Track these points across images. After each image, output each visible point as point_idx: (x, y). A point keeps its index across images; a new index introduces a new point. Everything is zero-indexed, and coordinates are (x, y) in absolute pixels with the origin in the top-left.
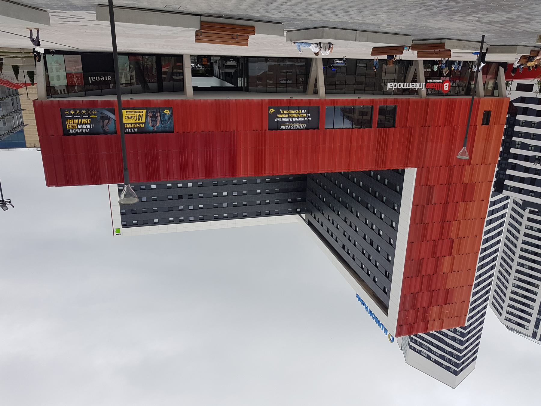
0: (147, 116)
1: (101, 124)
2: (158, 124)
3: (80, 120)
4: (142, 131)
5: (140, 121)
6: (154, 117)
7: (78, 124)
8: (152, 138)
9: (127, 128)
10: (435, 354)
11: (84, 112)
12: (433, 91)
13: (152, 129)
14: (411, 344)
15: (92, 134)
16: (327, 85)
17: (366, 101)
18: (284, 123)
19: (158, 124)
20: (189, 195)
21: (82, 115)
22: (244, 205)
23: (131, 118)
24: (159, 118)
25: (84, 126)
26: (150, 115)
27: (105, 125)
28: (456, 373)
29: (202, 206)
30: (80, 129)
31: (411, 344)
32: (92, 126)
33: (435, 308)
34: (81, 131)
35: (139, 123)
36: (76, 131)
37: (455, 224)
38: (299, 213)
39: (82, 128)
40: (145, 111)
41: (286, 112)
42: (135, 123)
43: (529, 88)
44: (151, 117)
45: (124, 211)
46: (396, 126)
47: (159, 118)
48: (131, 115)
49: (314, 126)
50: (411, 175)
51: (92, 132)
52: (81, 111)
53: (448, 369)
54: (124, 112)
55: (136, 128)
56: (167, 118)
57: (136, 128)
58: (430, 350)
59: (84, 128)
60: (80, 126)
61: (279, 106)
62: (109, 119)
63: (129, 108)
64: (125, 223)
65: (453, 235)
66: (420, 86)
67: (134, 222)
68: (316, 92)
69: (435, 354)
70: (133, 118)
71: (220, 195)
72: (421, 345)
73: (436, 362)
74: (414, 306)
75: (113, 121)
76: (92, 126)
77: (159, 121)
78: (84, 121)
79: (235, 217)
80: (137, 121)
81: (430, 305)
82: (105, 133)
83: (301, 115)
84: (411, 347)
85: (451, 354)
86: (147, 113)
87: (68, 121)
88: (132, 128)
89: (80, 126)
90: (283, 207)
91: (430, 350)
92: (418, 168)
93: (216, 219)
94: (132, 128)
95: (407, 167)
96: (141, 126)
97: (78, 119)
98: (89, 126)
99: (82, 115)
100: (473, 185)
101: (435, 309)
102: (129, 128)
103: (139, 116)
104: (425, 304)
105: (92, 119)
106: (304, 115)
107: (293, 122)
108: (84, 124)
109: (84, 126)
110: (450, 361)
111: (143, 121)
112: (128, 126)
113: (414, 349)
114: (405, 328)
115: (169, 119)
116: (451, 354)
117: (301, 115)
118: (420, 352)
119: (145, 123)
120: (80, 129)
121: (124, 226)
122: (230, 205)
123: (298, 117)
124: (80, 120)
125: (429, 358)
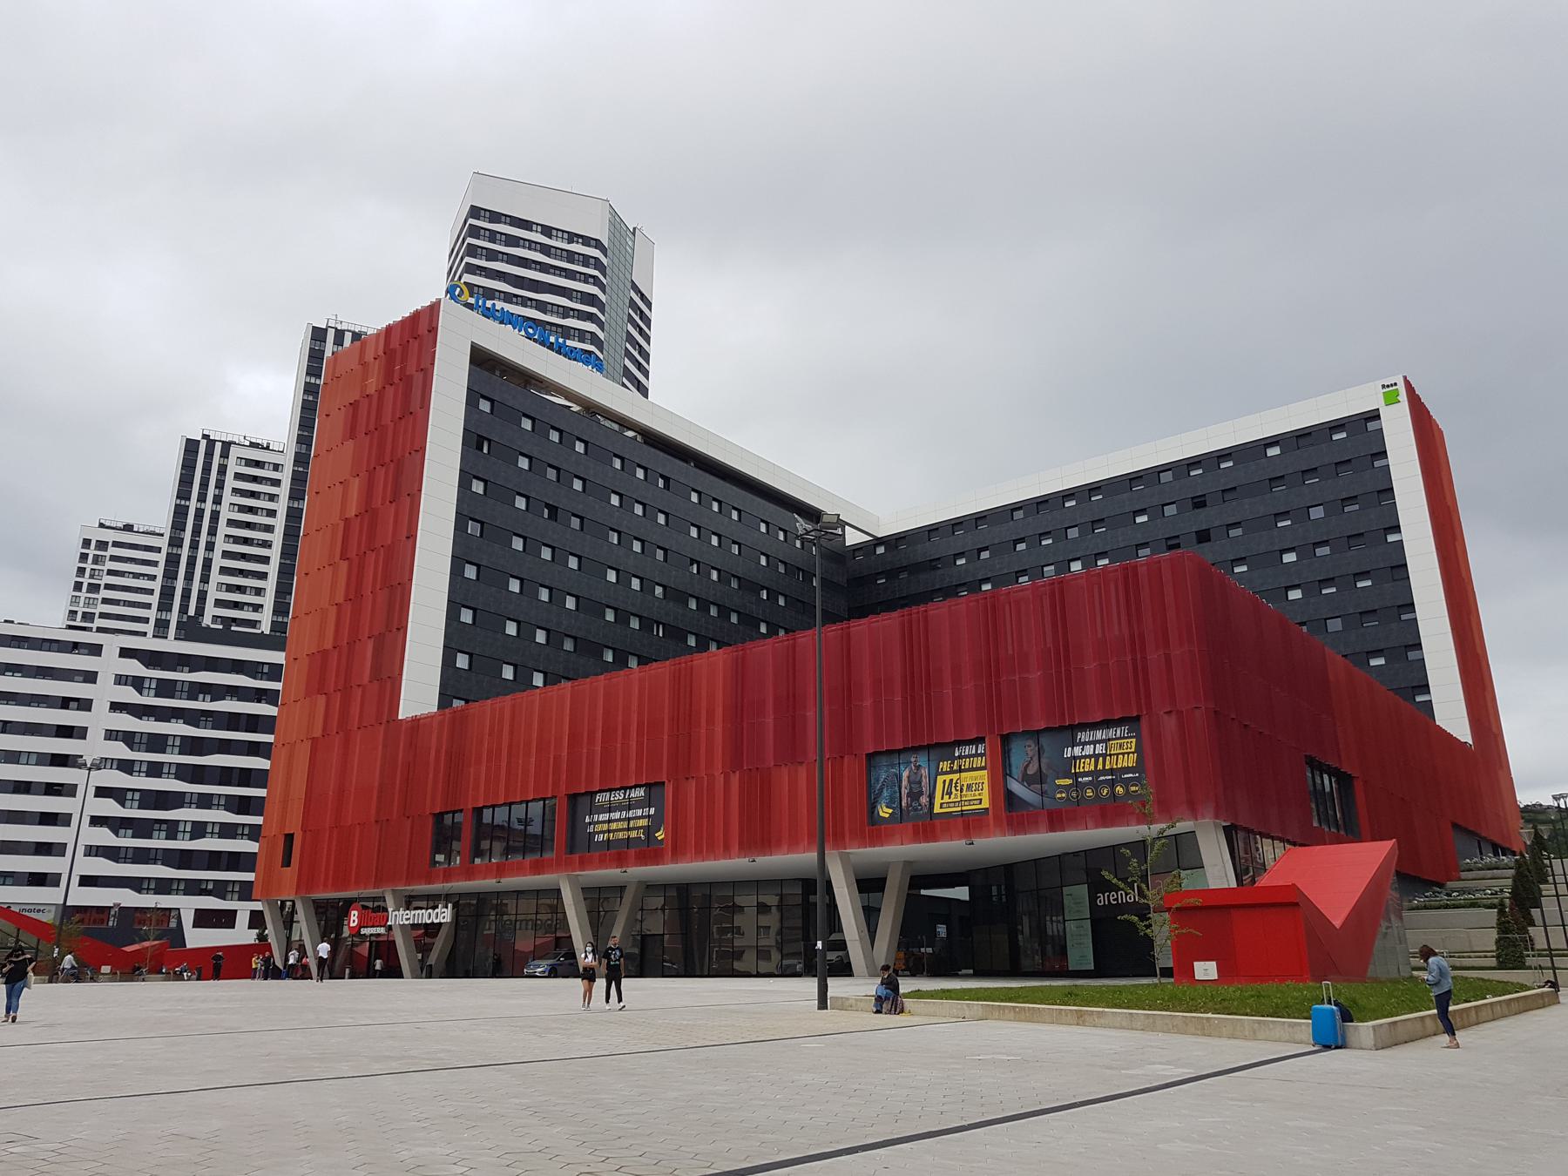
0: (932, 797)
1: (1044, 760)
2: (905, 774)
3: (1100, 767)
4: (942, 748)
5: (948, 778)
6: (914, 795)
7: (1104, 756)
8: (1168, 719)
9: (981, 755)
10: (531, 245)
11: (1089, 793)
12: (376, 911)
13: (922, 759)
14: (596, 253)
15: (1062, 728)
16: (557, 909)
17: (519, 870)
18: (639, 804)
19: (905, 774)
20: (1178, 546)
21: (1096, 785)
22: (1021, 540)
23: (969, 787)
24: (904, 792)
25: (1089, 750)
26: (924, 800)
27: (1036, 759)
28: (475, 212)
29: (1139, 520)
30: (1100, 742)
31: (596, 253)
32: (1068, 753)
33: (372, 390)
34: (1099, 735)
35: (952, 772)
36: (1111, 733)
37: (340, 599)
38: (879, 541)
39: (1095, 743)
40: (937, 810)
41: (633, 834)
42: (960, 771)
43: (205, 919)
44: (921, 793)
45: (1377, 464)
46: (431, 820)
47: (904, 792)
48: (969, 795)
49: (579, 801)
50: (419, 693)
51: (1069, 732)
52: (1098, 796)
53: (495, 217)
54: (986, 804)
55: (960, 757)
56: (885, 793)
57: (960, 757)
58: (545, 250)
59: (1089, 743)
60: (1100, 749)
61: (648, 851)
62: (1027, 780)
63: (974, 813)
64: (1371, 426)
65: (344, 565)
66: (400, 917)
67: (1344, 435)
68: (870, 885)
69: (531, 245)
70: (966, 785)
71: (1090, 560)
72: (571, 256)
73: (526, 225)
74: (407, 380)
75: (1014, 771)
76: (1068, 753)
77: (905, 783)
78: (1089, 766)
79: (1041, 503)
80: (955, 777)
81: (381, 392)
82: (1027, 734)
83: (605, 827)
84: (598, 244)
85: (492, 255)
86: (931, 804)
87: (1130, 761)
88: (969, 756)
89: (1100, 749)
90: (938, 548)
91: (545, 250)
92: (396, 720)
93: (1093, 488)
94: (969, 756)
95: (430, 717)
96: (945, 766)
97: (1104, 772)
98: (1077, 751)
99: (1096, 785)
100: (308, 694)
101: (373, 384)
102: (977, 755)
103: (950, 794)
104: (390, 391)
105: (1067, 775)
106: (599, 828)
107: (620, 808)
108: (1090, 757)
109: (1089, 750)
110: (493, 236)
111: (940, 779)
112: (979, 762)
113: (586, 241)
114: (423, 328)
115: (881, 790)
116: (492, 255)
117: (605, 827)
118: (572, 237)
119: (938, 774)
120: (1100, 742)
121: (1375, 416)
122: (1060, 534)
123: (609, 821)
124: (1100, 767)
125: (547, 231)
